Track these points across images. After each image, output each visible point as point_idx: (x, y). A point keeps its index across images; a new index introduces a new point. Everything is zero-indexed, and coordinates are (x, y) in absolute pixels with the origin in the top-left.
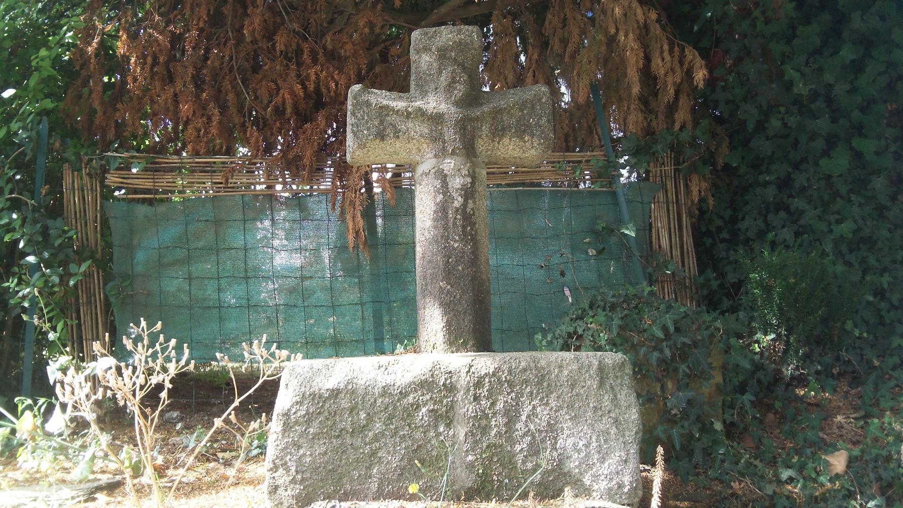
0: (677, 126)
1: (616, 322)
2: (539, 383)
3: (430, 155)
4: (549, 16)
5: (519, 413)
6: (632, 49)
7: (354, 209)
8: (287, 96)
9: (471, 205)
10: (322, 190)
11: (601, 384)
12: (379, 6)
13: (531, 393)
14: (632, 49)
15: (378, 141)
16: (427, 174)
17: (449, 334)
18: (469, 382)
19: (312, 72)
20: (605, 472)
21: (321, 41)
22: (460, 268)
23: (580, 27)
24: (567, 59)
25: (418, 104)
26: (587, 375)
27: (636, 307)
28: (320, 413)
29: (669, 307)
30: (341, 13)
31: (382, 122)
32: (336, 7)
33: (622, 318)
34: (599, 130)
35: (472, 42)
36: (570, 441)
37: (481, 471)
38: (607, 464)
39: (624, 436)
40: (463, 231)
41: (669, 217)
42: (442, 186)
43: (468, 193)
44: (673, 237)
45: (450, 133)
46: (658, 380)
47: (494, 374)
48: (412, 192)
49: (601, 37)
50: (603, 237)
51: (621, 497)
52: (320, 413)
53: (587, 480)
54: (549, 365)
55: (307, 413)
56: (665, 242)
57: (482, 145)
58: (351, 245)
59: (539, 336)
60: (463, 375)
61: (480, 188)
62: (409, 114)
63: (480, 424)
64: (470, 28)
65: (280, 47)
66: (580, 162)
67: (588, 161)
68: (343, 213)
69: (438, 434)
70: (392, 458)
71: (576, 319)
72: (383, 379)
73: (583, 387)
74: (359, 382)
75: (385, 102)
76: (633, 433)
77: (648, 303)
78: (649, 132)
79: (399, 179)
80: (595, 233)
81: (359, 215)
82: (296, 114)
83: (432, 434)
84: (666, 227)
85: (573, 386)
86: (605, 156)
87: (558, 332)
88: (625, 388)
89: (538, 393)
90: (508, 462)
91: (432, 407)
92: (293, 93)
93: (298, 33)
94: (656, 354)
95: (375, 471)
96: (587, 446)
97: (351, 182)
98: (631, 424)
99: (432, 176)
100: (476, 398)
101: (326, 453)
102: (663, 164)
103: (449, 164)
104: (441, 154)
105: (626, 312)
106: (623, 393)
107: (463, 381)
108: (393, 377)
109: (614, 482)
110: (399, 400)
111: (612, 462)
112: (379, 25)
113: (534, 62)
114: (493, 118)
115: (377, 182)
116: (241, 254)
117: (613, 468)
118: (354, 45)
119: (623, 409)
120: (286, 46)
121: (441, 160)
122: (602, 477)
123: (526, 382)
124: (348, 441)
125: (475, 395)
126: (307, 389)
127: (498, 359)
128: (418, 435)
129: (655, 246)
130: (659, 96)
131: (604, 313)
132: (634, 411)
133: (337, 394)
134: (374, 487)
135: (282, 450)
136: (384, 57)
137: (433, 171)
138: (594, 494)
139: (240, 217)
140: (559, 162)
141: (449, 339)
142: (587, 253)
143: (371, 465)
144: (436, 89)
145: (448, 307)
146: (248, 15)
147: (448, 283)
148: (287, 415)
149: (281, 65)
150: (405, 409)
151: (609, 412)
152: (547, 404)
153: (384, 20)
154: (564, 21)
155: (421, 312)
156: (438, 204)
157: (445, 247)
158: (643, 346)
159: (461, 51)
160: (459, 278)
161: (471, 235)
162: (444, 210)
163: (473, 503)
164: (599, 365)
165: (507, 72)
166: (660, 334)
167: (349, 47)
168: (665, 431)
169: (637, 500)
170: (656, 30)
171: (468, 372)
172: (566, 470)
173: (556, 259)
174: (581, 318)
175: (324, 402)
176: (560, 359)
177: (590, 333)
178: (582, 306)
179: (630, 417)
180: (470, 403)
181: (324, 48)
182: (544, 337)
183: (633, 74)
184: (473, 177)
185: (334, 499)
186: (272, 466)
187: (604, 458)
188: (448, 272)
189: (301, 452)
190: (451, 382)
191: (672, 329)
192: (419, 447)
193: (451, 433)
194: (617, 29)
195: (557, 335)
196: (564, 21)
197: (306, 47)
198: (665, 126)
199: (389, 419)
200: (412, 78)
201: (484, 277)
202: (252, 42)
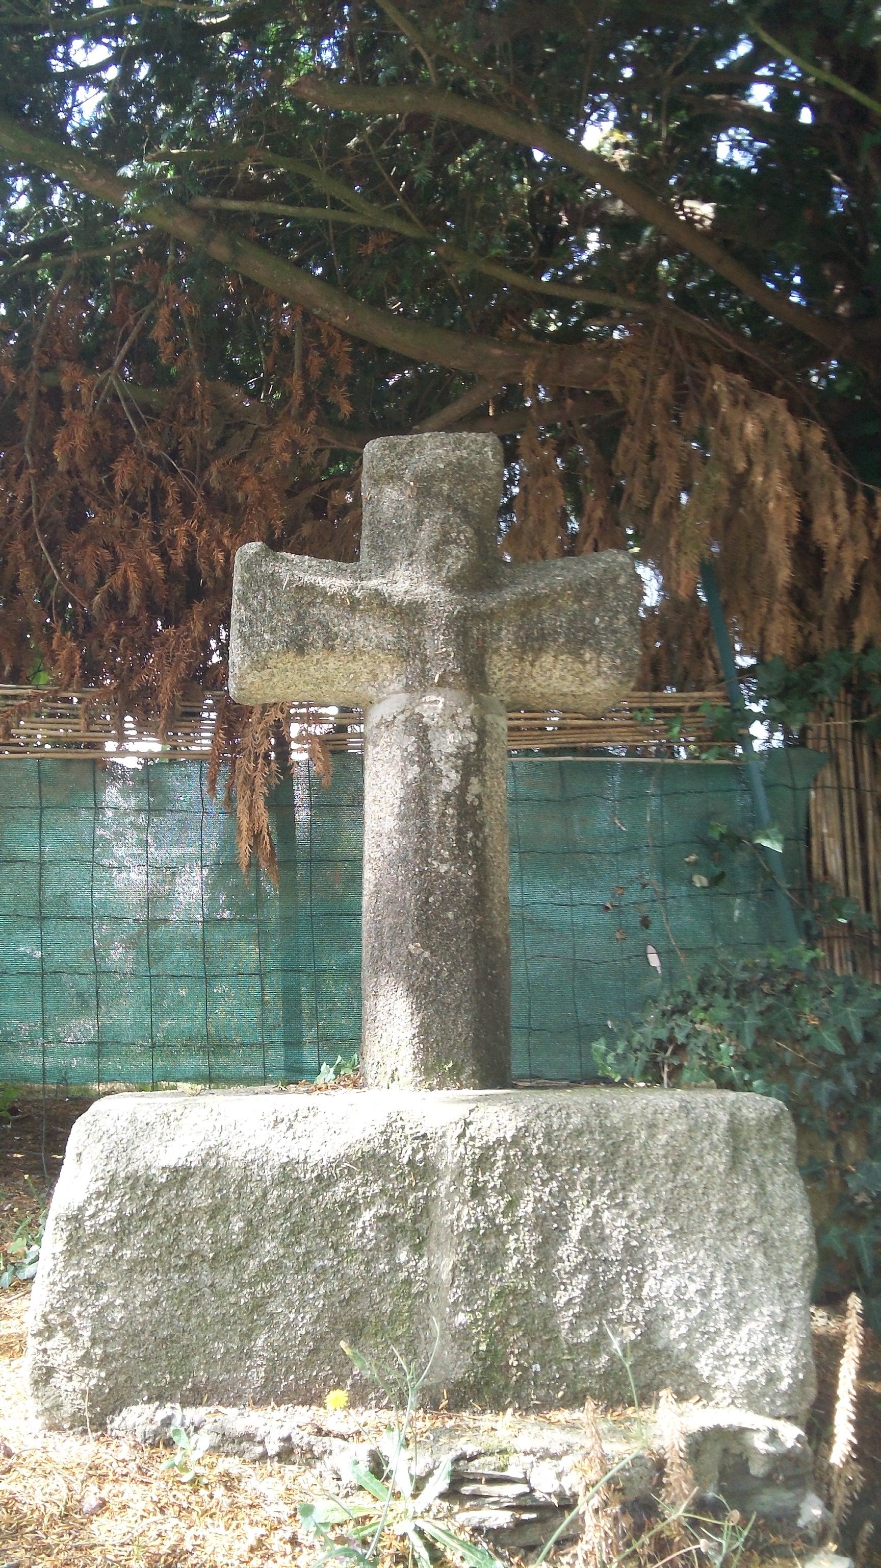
0: (858, 645)
1: (751, 1021)
2: (608, 1161)
3: (397, 686)
4: (624, 439)
5: (566, 1223)
6: (779, 497)
7: (253, 791)
8: (132, 575)
9: (475, 786)
10: (195, 753)
11: (735, 1163)
12: (312, 416)
13: (592, 1181)
14: (779, 497)
15: (291, 655)
16: (389, 725)
17: (425, 1050)
18: (462, 1158)
19: (180, 531)
20: (742, 1349)
21: (201, 477)
22: (450, 915)
23: (680, 461)
24: (656, 518)
25: (373, 583)
26: (706, 1143)
27: (788, 990)
28: (146, 1217)
29: (850, 993)
30: (241, 426)
31: (300, 618)
32: (231, 415)
33: (761, 1013)
34: (716, 651)
35: (482, 463)
36: (671, 1283)
37: (483, 1347)
38: (744, 1330)
39: (779, 1272)
40: (458, 841)
41: (842, 817)
42: (418, 749)
43: (471, 763)
44: (850, 853)
45: (437, 643)
46: (831, 1135)
47: (515, 1142)
48: (361, 760)
49: (719, 477)
50: (722, 852)
51: (773, 1402)
52: (146, 1217)
53: (704, 1365)
54: (628, 1122)
55: (120, 1217)
56: (834, 863)
57: (499, 668)
58: (245, 861)
59: (600, 1046)
60: (451, 1141)
61: (494, 756)
62: (355, 602)
63: (485, 1246)
64: (480, 437)
65: (121, 483)
66: (678, 710)
67: (694, 709)
68: (230, 800)
69: (396, 1268)
70: (297, 1317)
71: (673, 1012)
72: (282, 1149)
73: (699, 1168)
74: (232, 1154)
75: (308, 579)
76: (799, 1266)
77: (810, 983)
78: (807, 654)
79: (341, 736)
80: (709, 846)
81: (261, 803)
82: (148, 608)
83: (383, 1267)
84: (837, 834)
85: (676, 1167)
86: (726, 698)
87: (638, 1038)
88: (782, 1169)
89: (605, 1182)
90: (541, 1327)
91: (383, 1211)
92: (142, 568)
93: (158, 460)
94: (828, 1085)
95: (260, 1342)
96: (703, 1294)
97: (248, 740)
98: (794, 1247)
99: (399, 727)
100: (477, 1192)
101: (156, 1302)
102: (832, 715)
103: (434, 705)
104: (419, 683)
105: (769, 1001)
106: (779, 1180)
107: (450, 1155)
108: (304, 1143)
109: (760, 1370)
110: (314, 1194)
111: (755, 1329)
112: (311, 449)
113: (596, 524)
114: (523, 615)
115: (298, 740)
116: (32, 872)
117: (757, 1340)
118: (261, 482)
119: (779, 1214)
120: (132, 480)
121: (416, 695)
122: (736, 1360)
123: (581, 1158)
124: (206, 1277)
125: (474, 1185)
126: (121, 1167)
127: (523, 1109)
128: (354, 1269)
129: (817, 871)
130: (826, 587)
131: (727, 1003)
132: (801, 1218)
133: (184, 1179)
134: (257, 1376)
135: (64, 1294)
136: (318, 507)
137: (401, 717)
138: (718, 1395)
139: (32, 800)
140: (641, 710)
141: (424, 1062)
142: (691, 882)
143: (251, 1330)
144: (411, 555)
145: (424, 994)
146: (63, 423)
147: (426, 947)
148: (76, 1219)
149: (123, 518)
150: (328, 1214)
151: (751, 1221)
152: (624, 1205)
153: (321, 441)
154: (652, 451)
155: (368, 1004)
156: (408, 785)
157: (422, 872)
158: (802, 1069)
159: (461, 481)
160: (448, 937)
161: (475, 848)
162: (421, 797)
163: (465, 1414)
164: (731, 1122)
165: (545, 542)
166: (835, 1046)
167: (249, 486)
168: (843, 1238)
169: (805, 1406)
170: (822, 462)
171: (462, 1135)
172: (660, 1345)
173: (633, 895)
174: (681, 1011)
175: (157, 1194)
176: (650, 1110)
177: (701, 1041)
178: (684, 987)
179: (792, 1232)
180: (465, 1202)
181: (207, 489)
182: (611, 1047)
183: (778, 547)
184: (482, 731)
185: (171, 1399)
186: (42, 1325)
187: (738, 1319)
188: (427, 924)
189: (105, 1298)
190: (425, 1158)
191: (858, 1036)
192: (355, 1293)
193: (423, 1265)
194: (750, 463)
195: (635, 1045)
196: (652, 451)
197: (171, 487)
198: (836, 645)
199: (292, 1233)
200: (365, 532)
201: (498, 934)
202: (69, 472)
